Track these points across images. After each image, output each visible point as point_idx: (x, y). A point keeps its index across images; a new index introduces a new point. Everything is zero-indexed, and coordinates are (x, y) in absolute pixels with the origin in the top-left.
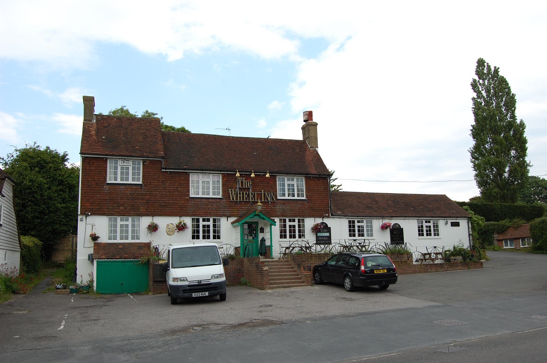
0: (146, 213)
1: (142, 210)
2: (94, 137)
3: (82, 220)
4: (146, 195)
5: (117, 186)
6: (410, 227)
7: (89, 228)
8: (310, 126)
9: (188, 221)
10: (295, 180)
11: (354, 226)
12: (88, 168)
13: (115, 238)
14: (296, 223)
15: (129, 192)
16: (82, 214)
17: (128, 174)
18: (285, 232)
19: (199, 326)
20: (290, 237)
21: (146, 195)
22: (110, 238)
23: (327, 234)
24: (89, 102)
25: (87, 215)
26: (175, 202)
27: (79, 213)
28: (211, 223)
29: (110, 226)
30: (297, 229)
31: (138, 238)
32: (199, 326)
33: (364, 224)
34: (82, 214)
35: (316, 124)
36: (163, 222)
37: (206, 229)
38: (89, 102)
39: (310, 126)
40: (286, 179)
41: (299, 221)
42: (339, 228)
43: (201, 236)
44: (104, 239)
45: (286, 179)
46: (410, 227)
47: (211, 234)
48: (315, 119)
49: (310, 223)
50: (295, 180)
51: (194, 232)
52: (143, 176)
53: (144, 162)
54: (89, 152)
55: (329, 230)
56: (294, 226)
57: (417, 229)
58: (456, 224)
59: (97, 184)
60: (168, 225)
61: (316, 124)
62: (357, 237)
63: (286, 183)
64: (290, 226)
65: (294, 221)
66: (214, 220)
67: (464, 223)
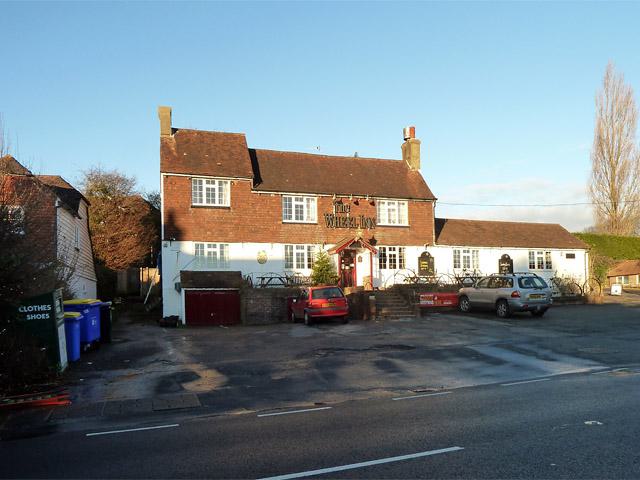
1: (231, 235)
2: (175, 153)
3: (166, 246)
4: (234, 219)
5: (203, 210)
8: (409, 145)
11: (459, 257)
15: (216, 216)
19: (324, 349)
21: (234, 219)
24: (166, 115)
28: (397, 253)
32: (324, 349)
34: (165, 240)
39: (409, 145)
47: (306, 263)
57: (452, 259)
61: (418, 143)
63: (205, 186)
66: (222, 247)
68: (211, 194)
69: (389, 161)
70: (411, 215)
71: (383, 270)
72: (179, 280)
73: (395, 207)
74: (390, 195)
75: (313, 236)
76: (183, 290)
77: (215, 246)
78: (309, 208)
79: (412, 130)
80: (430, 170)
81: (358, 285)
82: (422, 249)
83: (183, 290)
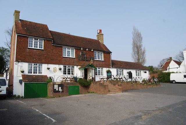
0: (45, 62)
1: (43, 61)
5: (33, 50)
6: (133, 72)
7: (19, 68)
9: (62, 67)
10: (71, 49)
11: (118, 73)
12: (20, 40)
13: (31, 73)
14: (100, 70)
16: (16, 61)
17: (37, 45)
18: (66, 71)
20: (68, 74)
22: (29, 73)
23: (110, 74)
24: (17, 13)
25: (19, 62)
26: (56, 59)
27: (15, 61)
29: (29, 67)
30: (38, 68)
31: (41, 73)
33: (100, 70)
35: (103, 35)
36: (52, 66)
37: (69, 71)
38: (17, 13)
40: (67, 48)
41: (72, 67)
42: (114, 71)
43: (98, 74)
44: (26, 73)
45: (67, 48)
46: (133, 72)
48: (102, 33)
49: (105, 70)
50: (71, 49)
51: (64, 71)
52: (44, 46)
53: (44, 40)
54: (20, 33)
55: (111, 72)
56: (100, 71)
58: (145, 72)
59: (23, 48)
60: (54, 68)
61: (103, 35)
62: (101, 75)
64: (98, 70)
65: (70, 67)
67: (147, 72)
68: (36, 45)
69: (80, 37)
70: (104, 57)
71: (96, 76)
72: (21, 78)
73: (70, 50)
74: (69, 46)
75: (74, 62)
76: (23, 83)
77: (70, 67)
78: (69, 53)
79: (101, 31)
80: (107, 43)
81: (22, 79)
82: (108, 69)
83: (23, 83)
